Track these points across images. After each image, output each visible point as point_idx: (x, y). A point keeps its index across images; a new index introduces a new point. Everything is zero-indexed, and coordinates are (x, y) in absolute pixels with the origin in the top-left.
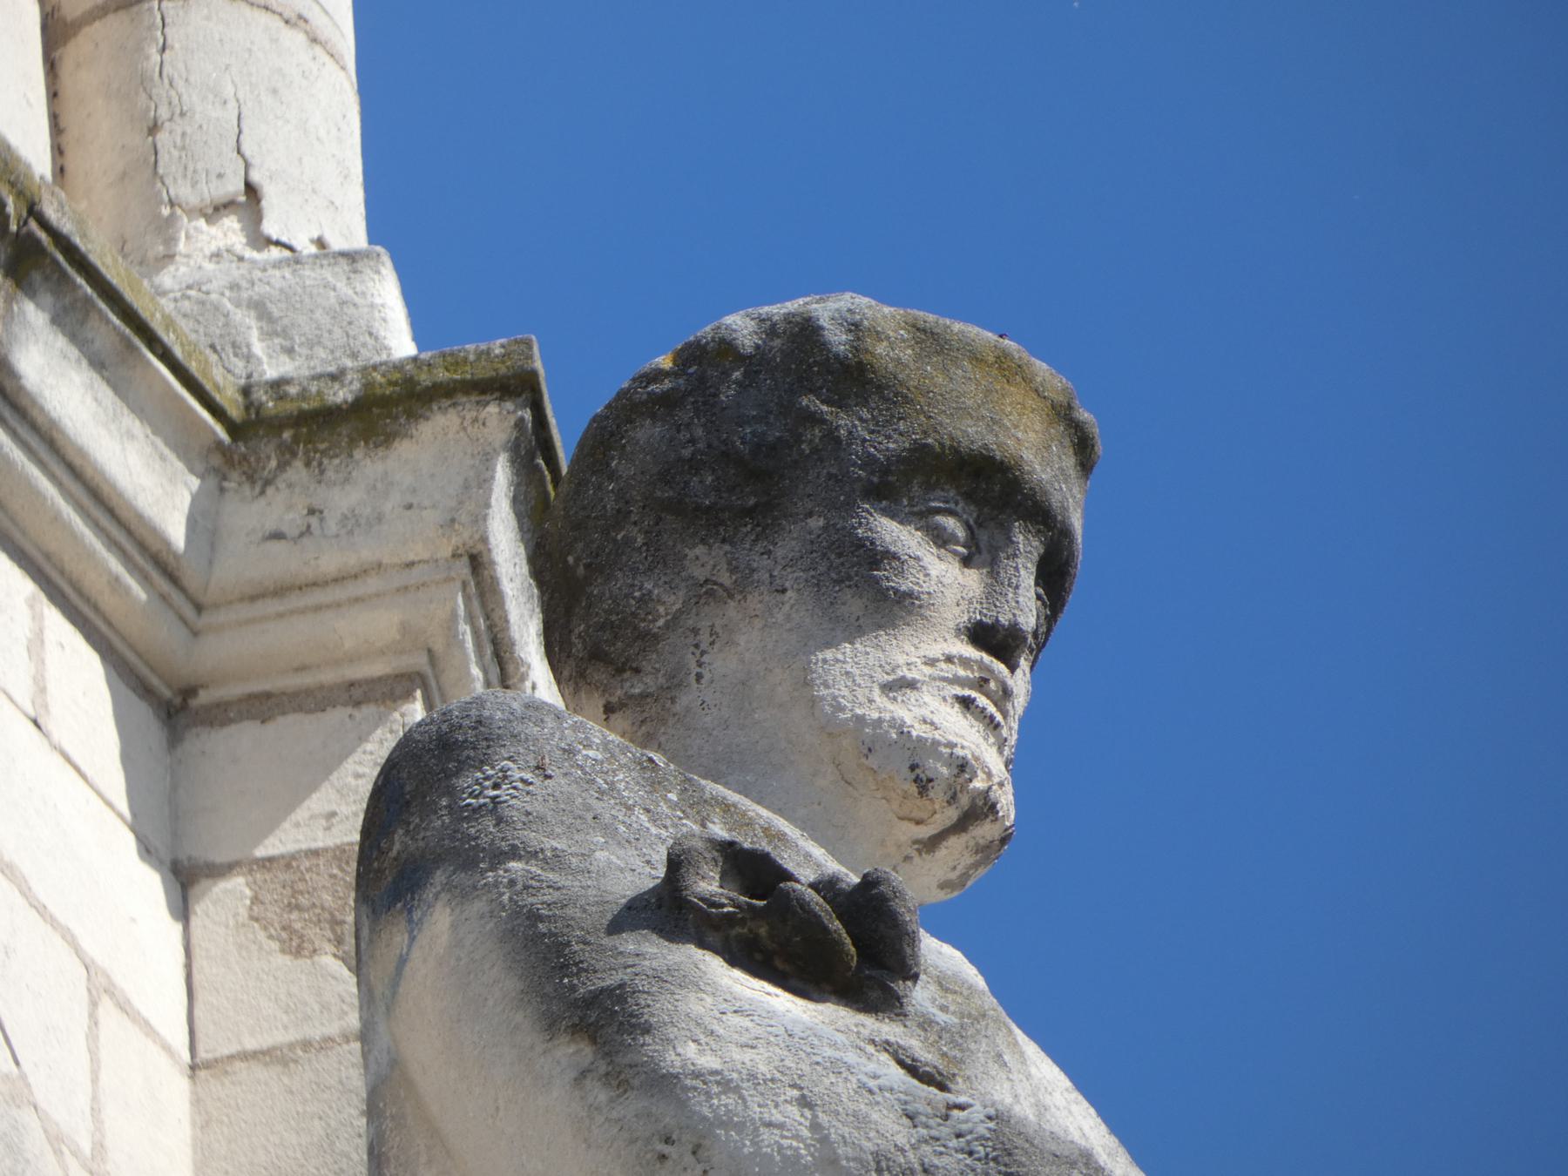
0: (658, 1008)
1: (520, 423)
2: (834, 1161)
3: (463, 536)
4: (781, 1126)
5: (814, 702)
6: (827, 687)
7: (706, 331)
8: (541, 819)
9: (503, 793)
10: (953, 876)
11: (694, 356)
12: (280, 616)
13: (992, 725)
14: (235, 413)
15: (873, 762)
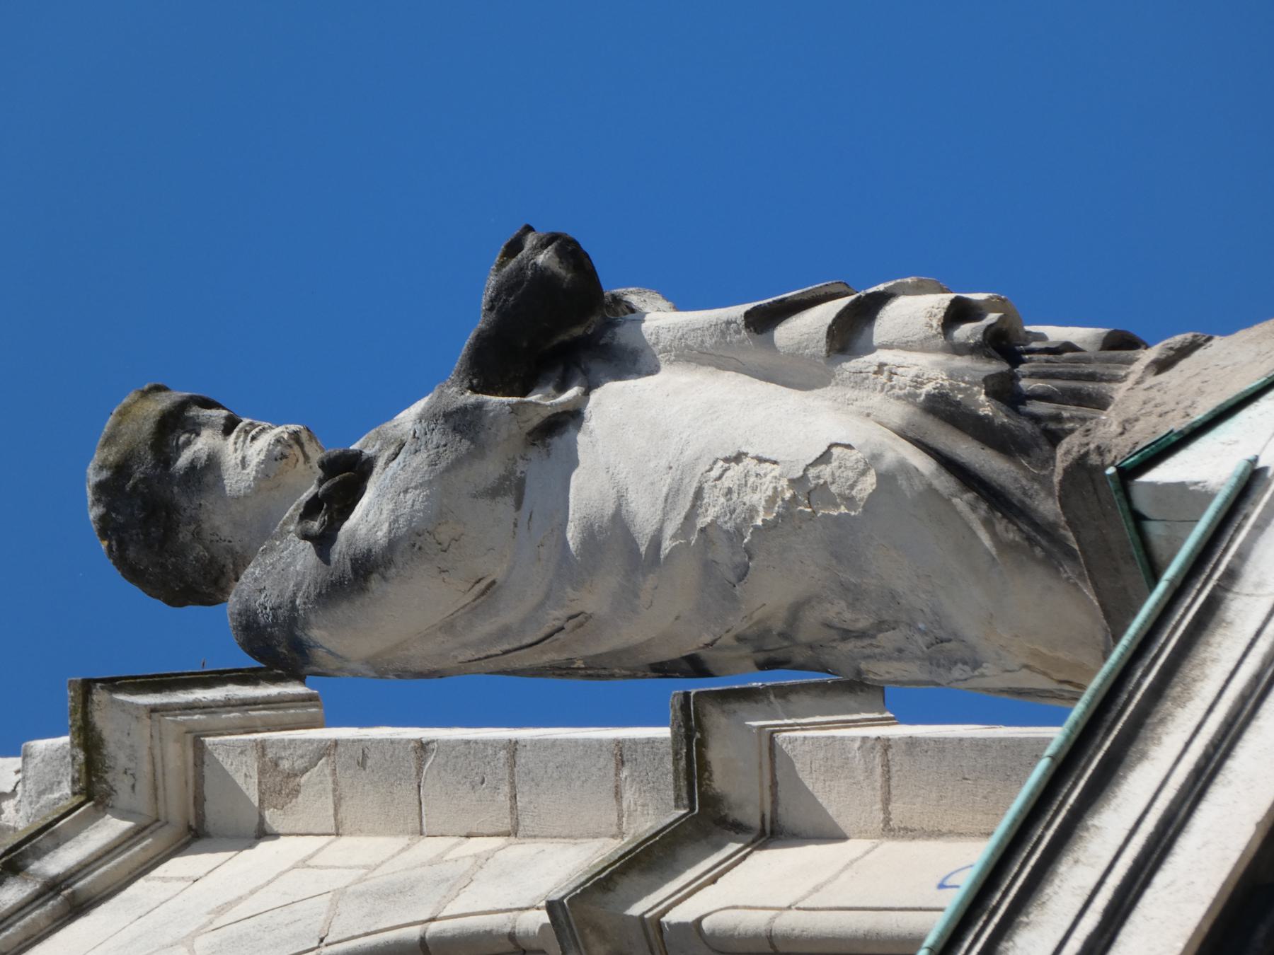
0: (362, 545)
1: (102, 688)
2: (430, 482)
3: (144, 715)
5: (245, 496)
7: (94, 527)
8: (281, 591)
9: (269, 605)
11: (104, 533)
12: (165, 789)
13: (263, 430)
14: (82, 798)
15: (272, 475)
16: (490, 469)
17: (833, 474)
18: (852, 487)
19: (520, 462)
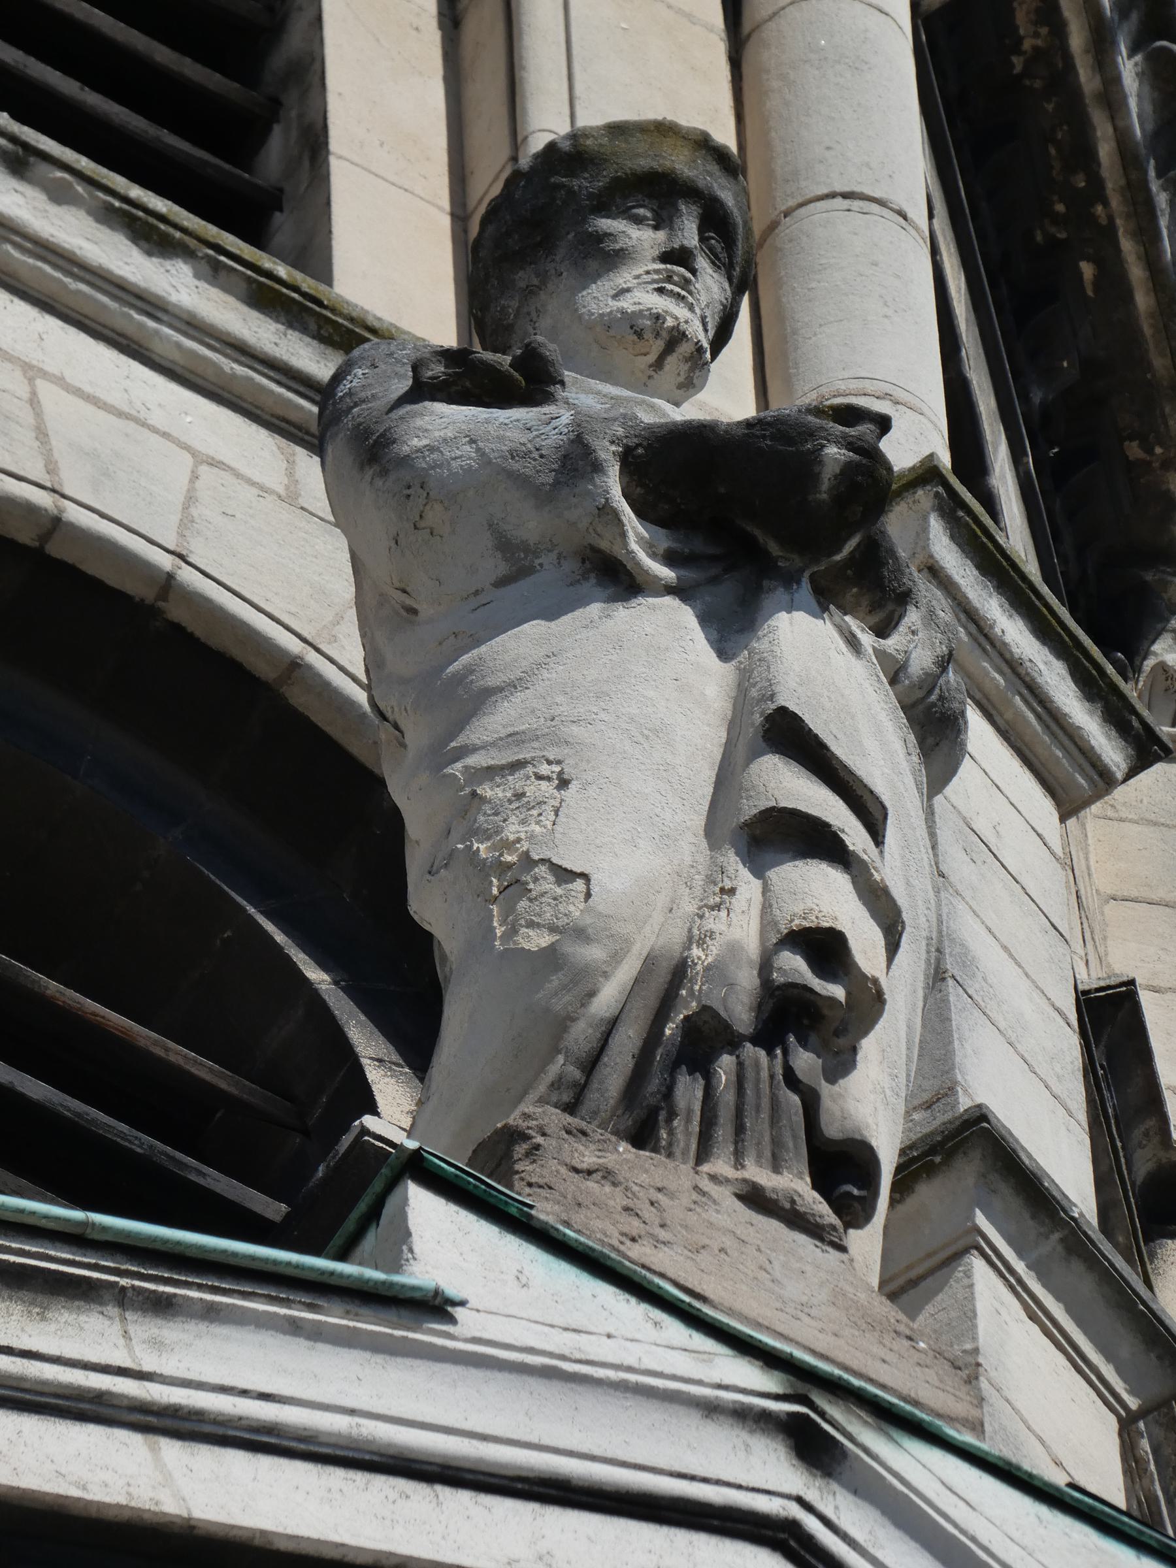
1: (937, 495)
2: (490, 462)
4: (461, 457)
5: (580, 317)
6: (584, 307)
10: (681, 379)
15: (612, 332)
16: (530, 524)
17: (543, 894)
18: (531, 925)
19: (553, 556)
